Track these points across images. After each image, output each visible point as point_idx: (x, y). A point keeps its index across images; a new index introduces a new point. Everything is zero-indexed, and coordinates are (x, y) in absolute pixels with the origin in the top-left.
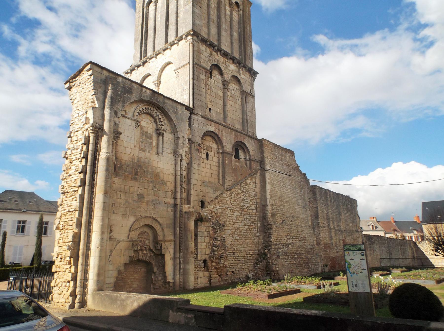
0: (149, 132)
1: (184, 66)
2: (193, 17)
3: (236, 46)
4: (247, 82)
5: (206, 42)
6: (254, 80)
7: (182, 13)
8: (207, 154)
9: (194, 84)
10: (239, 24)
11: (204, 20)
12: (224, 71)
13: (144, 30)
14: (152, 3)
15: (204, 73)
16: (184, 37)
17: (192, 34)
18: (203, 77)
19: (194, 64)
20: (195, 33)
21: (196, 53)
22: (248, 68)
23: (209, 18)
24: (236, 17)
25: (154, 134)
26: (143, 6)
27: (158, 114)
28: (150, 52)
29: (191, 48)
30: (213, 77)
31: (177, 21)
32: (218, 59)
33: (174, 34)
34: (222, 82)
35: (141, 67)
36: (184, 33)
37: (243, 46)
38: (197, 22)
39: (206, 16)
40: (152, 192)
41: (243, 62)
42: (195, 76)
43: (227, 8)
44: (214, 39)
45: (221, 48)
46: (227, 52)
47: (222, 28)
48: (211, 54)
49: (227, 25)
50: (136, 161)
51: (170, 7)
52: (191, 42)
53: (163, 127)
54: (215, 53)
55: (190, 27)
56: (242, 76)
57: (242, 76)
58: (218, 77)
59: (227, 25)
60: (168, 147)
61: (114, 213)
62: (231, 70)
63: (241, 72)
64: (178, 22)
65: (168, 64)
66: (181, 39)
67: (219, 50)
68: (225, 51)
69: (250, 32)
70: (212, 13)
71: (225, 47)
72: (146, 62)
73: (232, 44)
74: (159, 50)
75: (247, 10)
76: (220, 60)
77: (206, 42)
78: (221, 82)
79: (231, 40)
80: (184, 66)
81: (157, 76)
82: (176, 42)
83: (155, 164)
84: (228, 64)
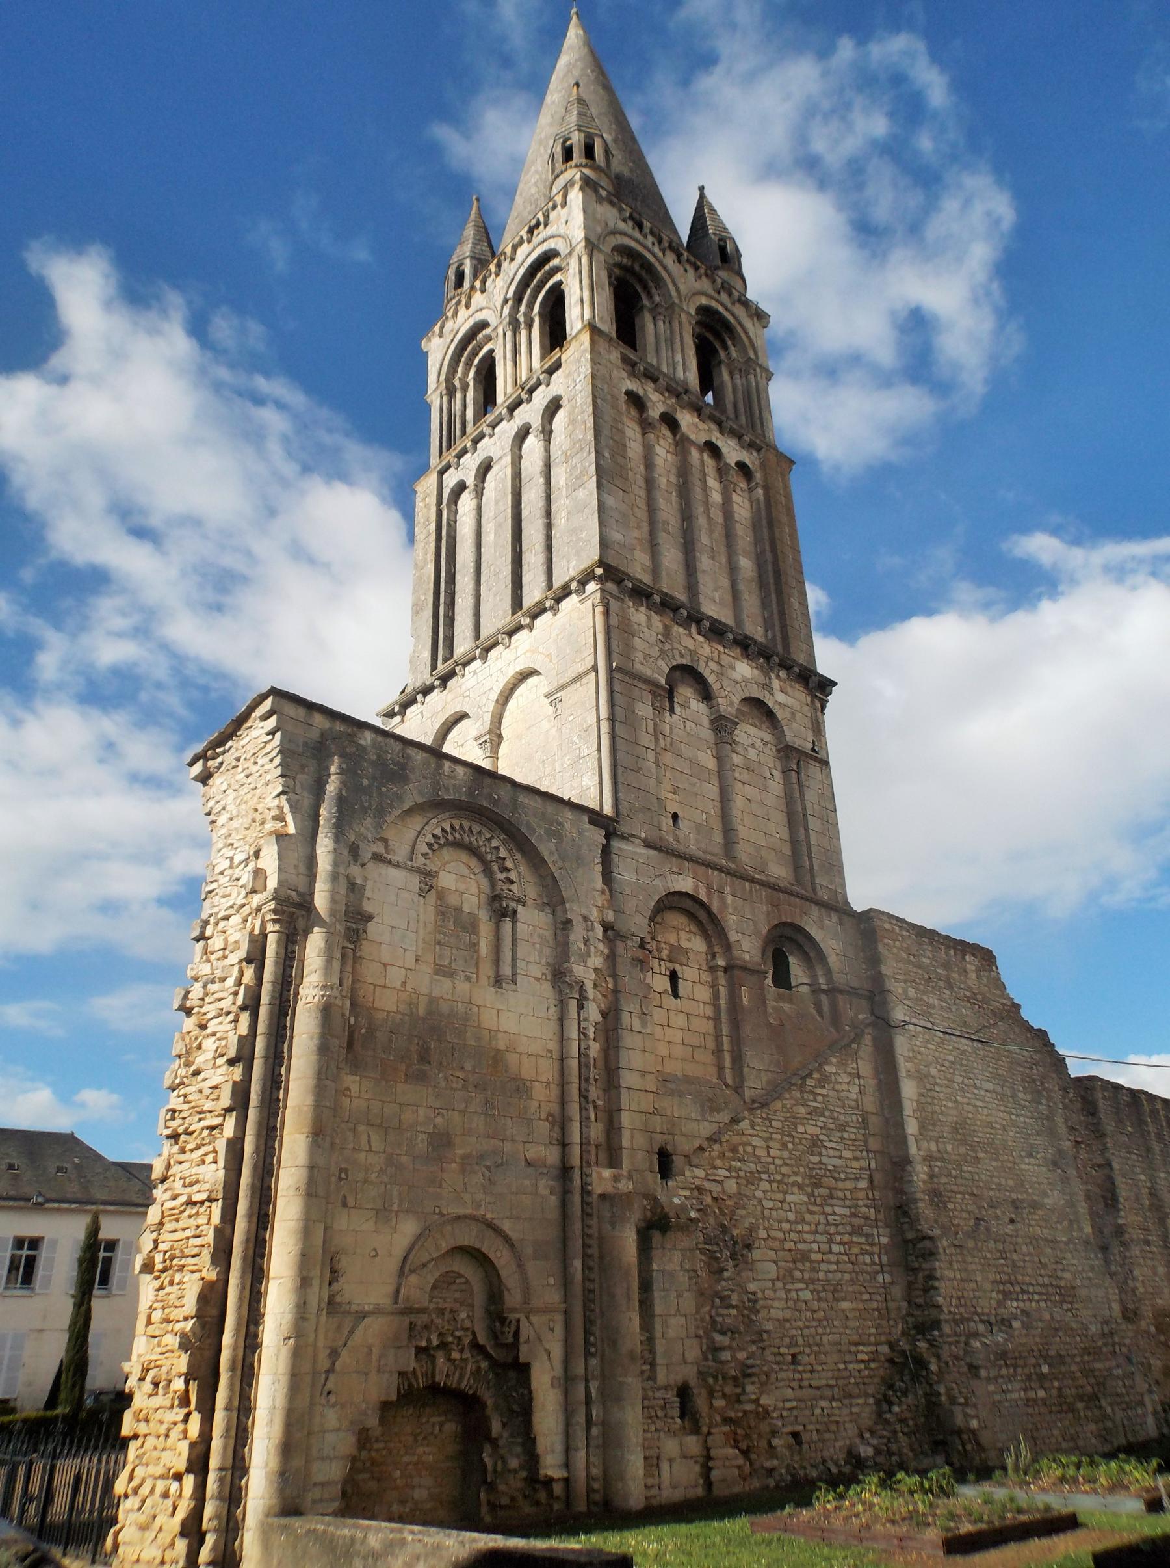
0: (466, 909)
1: (577, 678)
3: (751, 601)
4: (799, 716)
5: (649, 596)
6: (823, 708)
7: (564, 514)
8: (674, 977)
9: (613, 736)
11: (639, 527)
12: (715, 686)
13: (443, 574)
14: (467, 491)
15: (648, 697)
16: (574, 586)
17: (600, 577)
18: (644, 710)
19: (610, 671)
20: (610, 573)
21: (616, 634)
23: (652, 522)
24: (742, 509)
25: (483, 915)
27: (495, 843)
28: (463, 644)
31: (549, 538)
32: (692, 647)
33: (542, 578)
34: (712, 722)
36: (573, 573)
37: (773, 596)
38: (616, 536)
40: (479, 1123)
41: (780, 649)
43: (712, 482)
44: (673, 585)
45: (699, 611)
46: (719, 622)
47: (698, 546)
49: (716, 535)
50: (421, 1011)
51: (524, 498)
53: (514, 888)
54: (681, 630)
55: (594, 554)
56: (780, 697)
57: (780, 697)
58: (697, 706)
59: (716, 535)
60: (534, 957)
61: (345, 1204)
62: (739, 679)
63: (776, 683)
65: (525, 675)
66: (565, 592)
67: (695, 619)
68: (715, 623)
70: (662, 503)
71: (714, 607)
72: (451, 674)
73: (736, 595)
74: (494, 635)
76: (700, 651)
77: (649, 596)
80: (577, 678)
81: (487, 717)
82: (548, 604)
83: (488, 1020)
84: (726, 660)
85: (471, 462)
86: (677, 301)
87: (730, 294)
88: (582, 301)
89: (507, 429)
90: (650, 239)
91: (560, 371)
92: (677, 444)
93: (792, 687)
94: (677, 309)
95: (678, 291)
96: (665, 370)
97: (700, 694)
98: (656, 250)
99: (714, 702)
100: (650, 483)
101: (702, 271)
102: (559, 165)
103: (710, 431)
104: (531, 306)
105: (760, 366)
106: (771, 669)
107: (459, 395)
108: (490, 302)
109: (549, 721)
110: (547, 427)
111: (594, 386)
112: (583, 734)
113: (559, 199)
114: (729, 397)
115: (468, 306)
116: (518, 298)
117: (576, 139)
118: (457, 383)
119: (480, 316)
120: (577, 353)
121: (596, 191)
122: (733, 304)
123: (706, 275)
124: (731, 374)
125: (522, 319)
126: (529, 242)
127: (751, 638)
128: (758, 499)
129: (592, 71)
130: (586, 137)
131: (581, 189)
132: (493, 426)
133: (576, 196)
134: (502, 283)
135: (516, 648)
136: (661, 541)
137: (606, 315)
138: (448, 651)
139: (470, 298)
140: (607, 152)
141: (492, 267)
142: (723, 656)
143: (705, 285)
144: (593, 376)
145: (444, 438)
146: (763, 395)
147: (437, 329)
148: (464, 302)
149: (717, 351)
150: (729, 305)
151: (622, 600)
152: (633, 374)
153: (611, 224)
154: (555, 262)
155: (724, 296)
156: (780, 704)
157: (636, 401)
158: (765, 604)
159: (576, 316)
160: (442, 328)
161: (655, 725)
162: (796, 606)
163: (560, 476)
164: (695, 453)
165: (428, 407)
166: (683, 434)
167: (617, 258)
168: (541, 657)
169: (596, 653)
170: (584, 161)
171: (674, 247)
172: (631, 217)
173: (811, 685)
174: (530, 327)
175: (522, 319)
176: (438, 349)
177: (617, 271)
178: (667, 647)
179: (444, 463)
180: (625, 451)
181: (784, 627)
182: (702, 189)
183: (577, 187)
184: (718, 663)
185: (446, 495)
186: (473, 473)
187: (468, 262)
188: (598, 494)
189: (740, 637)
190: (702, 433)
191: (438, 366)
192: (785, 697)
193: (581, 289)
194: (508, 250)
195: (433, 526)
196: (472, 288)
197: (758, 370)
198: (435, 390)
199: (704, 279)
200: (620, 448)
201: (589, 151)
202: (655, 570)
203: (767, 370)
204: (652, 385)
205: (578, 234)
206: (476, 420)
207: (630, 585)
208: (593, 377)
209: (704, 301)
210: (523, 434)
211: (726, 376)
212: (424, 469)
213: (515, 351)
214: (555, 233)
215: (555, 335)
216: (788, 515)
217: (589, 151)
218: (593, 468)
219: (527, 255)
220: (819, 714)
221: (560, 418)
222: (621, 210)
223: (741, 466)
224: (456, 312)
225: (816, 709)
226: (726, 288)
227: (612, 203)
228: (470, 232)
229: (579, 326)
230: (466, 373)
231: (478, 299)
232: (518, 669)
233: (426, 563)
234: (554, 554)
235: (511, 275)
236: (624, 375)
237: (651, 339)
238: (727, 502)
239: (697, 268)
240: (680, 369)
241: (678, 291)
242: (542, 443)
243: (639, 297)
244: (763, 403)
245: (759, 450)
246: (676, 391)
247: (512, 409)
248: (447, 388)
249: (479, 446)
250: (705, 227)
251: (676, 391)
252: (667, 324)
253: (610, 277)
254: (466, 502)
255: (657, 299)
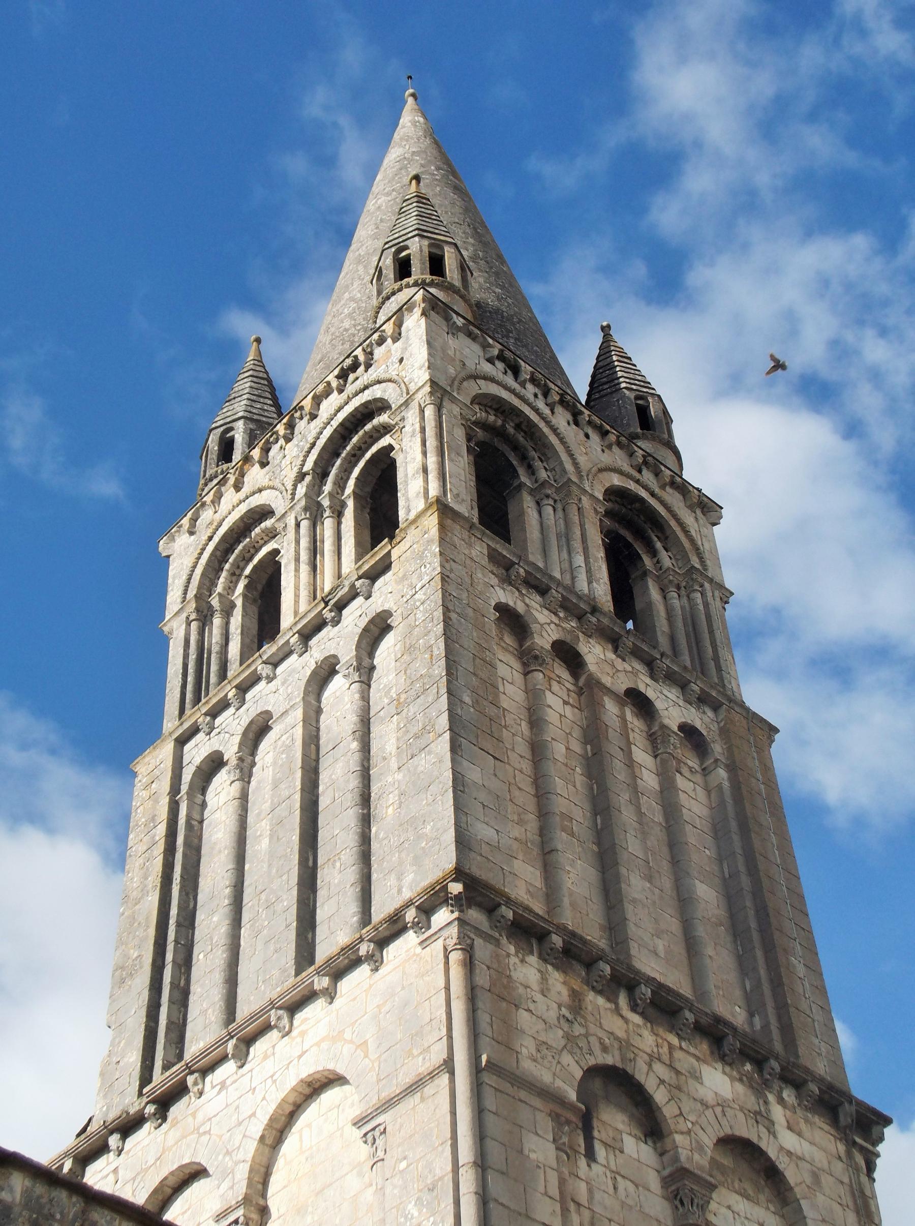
1: (415, 1087)
2: (458, 808)
3: (719, 960)
4: (826, 1180)
5: (542, 936)
6: (870, 1168)
7: (392, 798)
9: (484, 1200)
10: (716, 837)
11: (520, 822)
12: (669, 1111)
13: (174, 911)
14: (224, 772)
15: (546, 1125)
16: (410, 915)
17: (458, 897)
18: (541, 1149)
19: (477, 1070)
20: (473, 891)
21: (486, 1003)
22: (814, 1088)
23: (544, 814)
24: (694, 802)
26: (175, 789)
28: (203, 1030)
29: (457, 973)
30: (600, 1152)
31: (365, 840)
32: (621, 1034)
33: (352, 910)
34: (666, 1182)
35: (147, 1126)
36: (407, 894)
37: (759, 953)
38: (484, 831)
39: (530, 804)
41: (778, 1046)
42: (490, 1144)
43: (641, 755)
44: (581, 913)
45: (631, 968)
46: (669, 990)
47: (623, 857)
48: (576, 1005)
49: (652, 842)
51: (324, 778)
52: (451, 942)
54: (601, 1001)
55: (447, 859)
56: (789, 1140)
57: (789, 1140)
58: (636, 1148)
59: (652, 842)
62: (710, 1098)
63: (778, 1113)
64: (374, 846)
65: (317, 1086)
66: (395, 927)
67: (624, 982)
68: (659, 988)
69: (793, 876)
70: (559, 785)
71: (656, 958)
72: (179, 1091)
73: (691, 945)
74: (264, 1011)
75: (754, 763)
76: (636, 1041)
77: (542, 936)
78: (654, 1183)
79: (687, 926)
80: (415, 1087)
81: (242, 1173)
82: (364, 949)
84: (684, 1061)
85: (233, 724)
86: (574, 479)
87: (657, 474)
88: (425, 470)
89: (299, 668)
90: (531, 389)
91: (388, 576)
92: (580, 692)
93: (807, 1121)
94: (574, 488)
95: (576, 464)
96: (557, 575)
97: (640, 1125)
98: (541, 404)
99: (668, 1141)
100: (538, 751)
101: (612, 438)
102: (390, 284)
103: (635, 673)
104: (341, 484)
105: (711, 581)
106: (766, 1084)
107: (217, 621)
108: (275, 479)
109: (361, 1175)
110: (366, 662)
111: (445, 594)
112: (426, 1197)
113: (389, 328)
114: (662, 624)
115: (238, 487)
116: (321, 473)
117: (416, 248)
118: (215, 602)
119: (257, 501)
120: (418, 547)
121: (447, 319)
122: (663, 487)
123: (619, 444)
124: (663, 591)
125: (326, 503)
126: (340, 391)
127: (727, 1024)
128: (720, 787)
129: (438, 169)
130: (430, 246)
131: (424, 313)
132: (275, 663)
133: (416, 325)
134: (295, 451)
135: (303, 1034)
136: (560, 847)
137: (463, 491)
138: (173, 1051)
139: (242, 475)
140: (463, 267)
141: (281, 429)
142: (678, 1054)
143: (618, 457)
144: (444, 578)
145: (190, 687)
146: (717, 624)
147: (185, 522)
148: (232, 479)
149: (641, 558)
150: (657, 490)
151: (497, 943)
152: (507, 580)
153: (471, 365)
154: (383, 418)
155: (647, 476)
156: (789, 1153)
157: (513, 622)
158: (744, 966)
159: (414, 492)
160: (194, 520)
161: (562, 1182)
162: (801, 970)
163: (386, 738)
164: (611, 707)
165: (164, 641)
166: (591, 677)
167: (481, 415)
168: (347, 1049)
169: (450, 1037)
170: (428, 278)
171: (567, 401)
172: (501, 357)
173: (844, 1120)
174: (338, 514)
175: (326, 503)
176: (184, 553)
177: (480, 434)
178: (578, 1030)
179: (186, 725)
180: (496, 696)
181: (782, 1008)
182: (606, 329)
183: (417, 311)
184: (671, 1066)
185: (187, 775)
186: (237, 739)
187: (240, 425)
188: (453, 760)
189: (704, 1021)
190: (621, 675)
191: (185, 577)
192: (798, 1142)
193: (424, 453)
194: (307, 403)
195: (162, 829)
196: (247, 459)
197: (707, 585)
198: (177, 613)
199: (615, 449)
200: (488, 689)
201: (436, 265)
202: (552, 892)
203: (721, 586)
204: (538, 598)
205: (418, 373)
206: (244, 657)
207: (510, 915)
208: (443, 579)
209: (616, 480)
210: (326, 672)
211: (655, 594)
212: (150, 735)
213: (315, 550)
214: (383, 376)
215: (380, 518)
216: (772, 814)
217: (436, 265)
218: (443, 721)
219: (336, 409)
220: (864, 1179)
221: (388, 646)
222: (485, 346)
223: (688, 731)
224: (219, 496)
225: (857, 1169)
226: (651, 464)
227: (470, 335)
228: (244, 385)
229: (421, 505)
230: (230, 588)
231: (255, 476)
232: (304, 1075)
233: (144, 892)
234: (374, 867)
235: (311, 439)
236: (494, 581)
237: (533, 532)
238: (667, 789)
239: (604, 434)
240: (582, 577)
241: (576, 464)
242: (356, 686)
243: (515, 475)
244: (718, 634)
245: (716, 708)
246: (575, 608)
247: (307, 635)
248: (198, 610)
249: (249, 696)
250: (613, 379)
251: (575, 608)
252: (560, 513)
253: (469, 439)
254: (223, 788)
255: (543, 475)
